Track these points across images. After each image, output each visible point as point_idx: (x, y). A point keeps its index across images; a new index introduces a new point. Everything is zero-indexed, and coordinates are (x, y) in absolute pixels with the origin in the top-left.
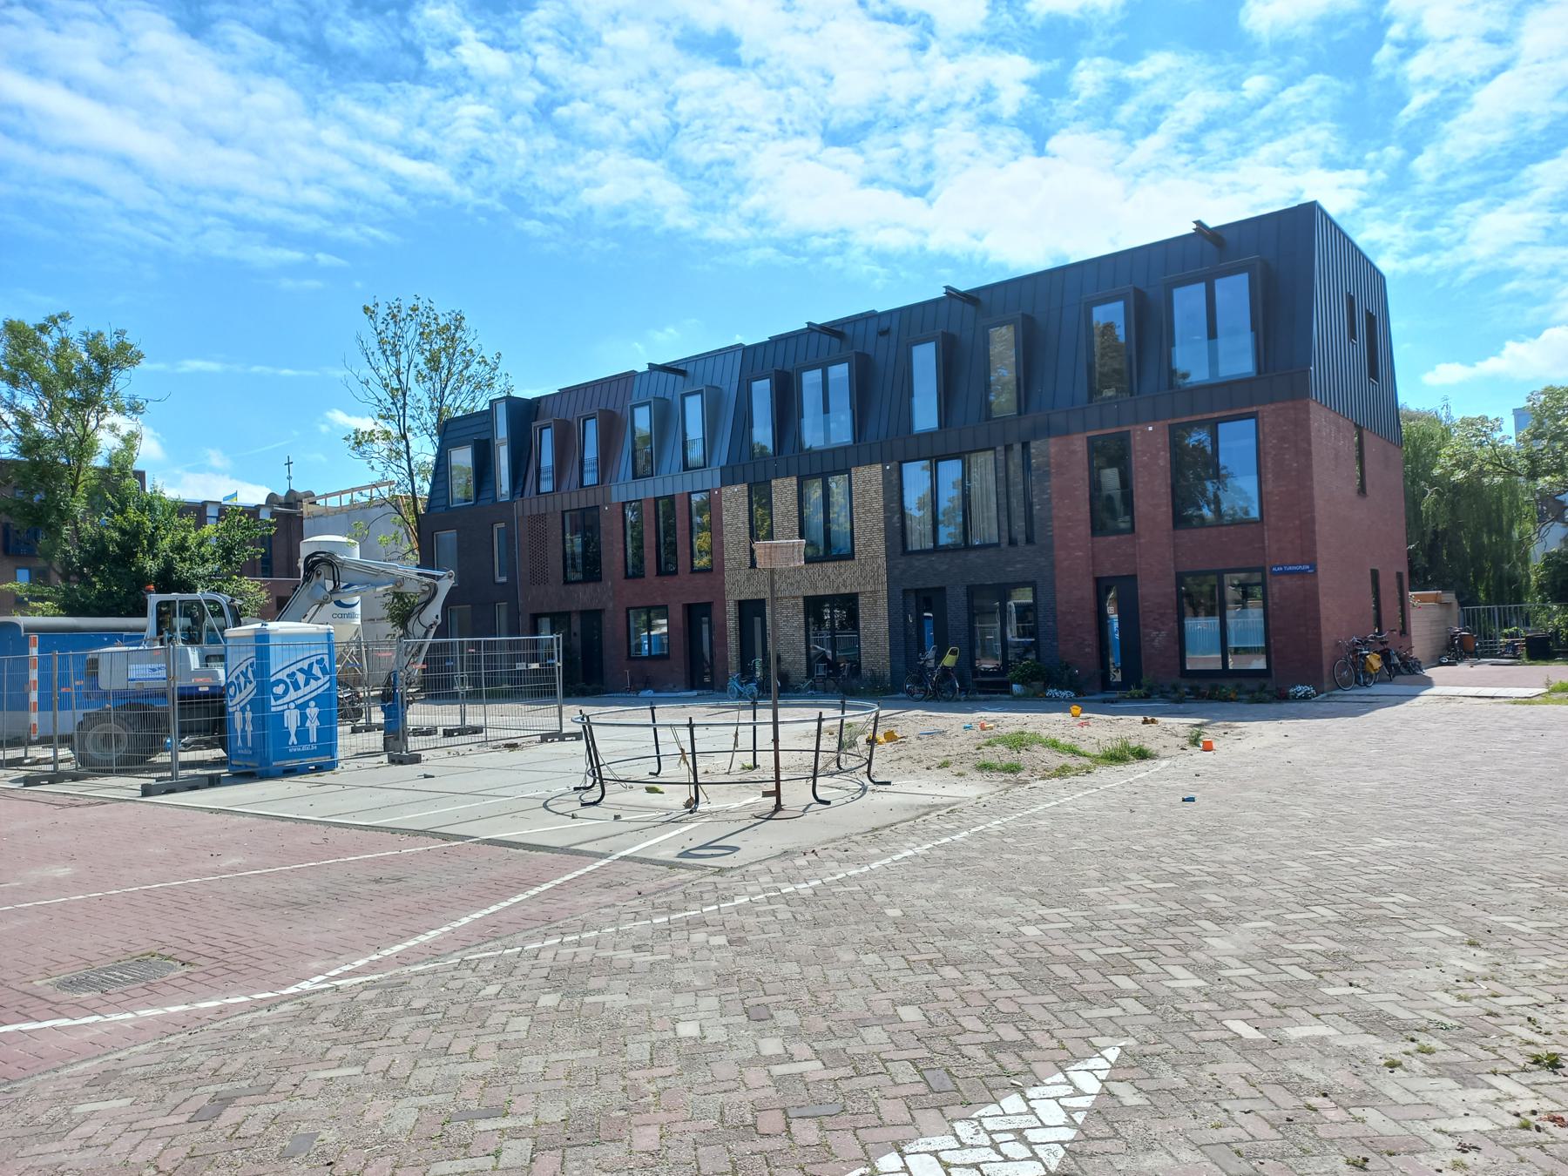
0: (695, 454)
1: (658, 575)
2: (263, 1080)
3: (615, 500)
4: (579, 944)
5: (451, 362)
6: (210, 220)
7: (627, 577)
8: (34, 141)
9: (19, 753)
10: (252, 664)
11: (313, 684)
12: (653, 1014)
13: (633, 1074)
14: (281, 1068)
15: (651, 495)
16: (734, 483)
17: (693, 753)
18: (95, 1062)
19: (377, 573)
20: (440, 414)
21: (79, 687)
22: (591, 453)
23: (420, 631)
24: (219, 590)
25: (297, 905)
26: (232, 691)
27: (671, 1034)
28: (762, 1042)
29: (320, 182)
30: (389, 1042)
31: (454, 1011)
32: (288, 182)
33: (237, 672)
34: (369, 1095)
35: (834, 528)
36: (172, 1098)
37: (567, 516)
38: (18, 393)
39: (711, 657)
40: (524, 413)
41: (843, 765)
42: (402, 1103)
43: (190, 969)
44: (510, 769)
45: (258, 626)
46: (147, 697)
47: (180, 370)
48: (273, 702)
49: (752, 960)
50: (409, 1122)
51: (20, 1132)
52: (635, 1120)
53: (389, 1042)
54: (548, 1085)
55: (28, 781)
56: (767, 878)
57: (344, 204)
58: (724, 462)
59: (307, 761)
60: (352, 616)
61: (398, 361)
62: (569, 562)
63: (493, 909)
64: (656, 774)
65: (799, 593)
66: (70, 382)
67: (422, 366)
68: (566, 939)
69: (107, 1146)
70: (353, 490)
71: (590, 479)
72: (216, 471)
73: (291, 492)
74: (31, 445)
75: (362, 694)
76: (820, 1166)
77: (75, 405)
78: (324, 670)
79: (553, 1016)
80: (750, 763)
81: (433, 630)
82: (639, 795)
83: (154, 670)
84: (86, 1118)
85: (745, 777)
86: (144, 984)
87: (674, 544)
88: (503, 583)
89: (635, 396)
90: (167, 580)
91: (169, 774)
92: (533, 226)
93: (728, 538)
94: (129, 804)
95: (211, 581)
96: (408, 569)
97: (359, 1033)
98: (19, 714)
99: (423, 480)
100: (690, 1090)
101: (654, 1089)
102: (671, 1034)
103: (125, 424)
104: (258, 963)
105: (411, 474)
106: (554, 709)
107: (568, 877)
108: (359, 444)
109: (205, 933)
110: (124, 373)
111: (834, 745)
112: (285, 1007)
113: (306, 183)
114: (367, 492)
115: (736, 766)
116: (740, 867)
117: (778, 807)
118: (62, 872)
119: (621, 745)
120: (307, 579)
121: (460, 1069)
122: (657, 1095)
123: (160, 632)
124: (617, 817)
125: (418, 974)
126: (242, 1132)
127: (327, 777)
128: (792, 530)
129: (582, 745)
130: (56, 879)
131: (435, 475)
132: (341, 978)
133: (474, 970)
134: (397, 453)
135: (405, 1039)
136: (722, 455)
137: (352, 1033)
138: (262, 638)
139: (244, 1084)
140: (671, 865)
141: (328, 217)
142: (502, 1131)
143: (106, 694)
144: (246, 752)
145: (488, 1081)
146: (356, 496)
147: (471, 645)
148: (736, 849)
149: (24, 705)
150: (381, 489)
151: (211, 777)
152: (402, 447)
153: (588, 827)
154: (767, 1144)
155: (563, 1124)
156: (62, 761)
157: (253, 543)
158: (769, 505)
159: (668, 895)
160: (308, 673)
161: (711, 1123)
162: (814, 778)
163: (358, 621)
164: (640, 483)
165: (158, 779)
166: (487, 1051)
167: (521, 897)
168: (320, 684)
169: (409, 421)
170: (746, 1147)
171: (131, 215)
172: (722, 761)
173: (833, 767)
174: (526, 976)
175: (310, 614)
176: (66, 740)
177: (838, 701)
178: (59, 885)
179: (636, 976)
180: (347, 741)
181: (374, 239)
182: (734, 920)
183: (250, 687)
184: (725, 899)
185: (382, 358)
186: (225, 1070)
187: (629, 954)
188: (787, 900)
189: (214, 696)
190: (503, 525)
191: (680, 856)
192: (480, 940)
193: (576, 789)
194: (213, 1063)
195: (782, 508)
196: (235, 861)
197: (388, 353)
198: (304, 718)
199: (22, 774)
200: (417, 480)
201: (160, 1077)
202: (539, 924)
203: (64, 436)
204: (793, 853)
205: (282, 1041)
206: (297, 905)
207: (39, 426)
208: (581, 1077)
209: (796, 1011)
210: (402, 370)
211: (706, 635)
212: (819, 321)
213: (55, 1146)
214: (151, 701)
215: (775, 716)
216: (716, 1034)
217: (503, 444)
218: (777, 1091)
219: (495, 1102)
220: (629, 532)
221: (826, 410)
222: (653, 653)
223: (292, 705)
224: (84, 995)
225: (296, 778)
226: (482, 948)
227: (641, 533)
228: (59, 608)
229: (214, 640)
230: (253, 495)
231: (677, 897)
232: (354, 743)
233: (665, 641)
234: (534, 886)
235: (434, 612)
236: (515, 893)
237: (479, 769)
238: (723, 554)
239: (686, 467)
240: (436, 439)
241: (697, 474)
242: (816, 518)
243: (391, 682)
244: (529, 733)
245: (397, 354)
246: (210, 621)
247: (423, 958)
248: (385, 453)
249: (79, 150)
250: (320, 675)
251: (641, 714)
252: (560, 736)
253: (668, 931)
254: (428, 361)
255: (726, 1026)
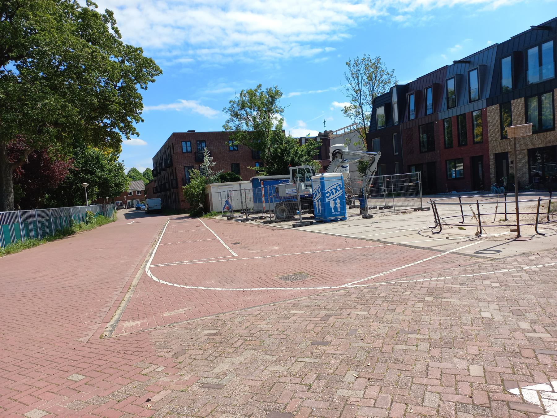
0: (475, 95)
1: (459, 146)
2: (339, 311)
3: (440, 118)
4: (438, 281)
5: (376, 77)
6: (293, 45)
7: (445, 148)
8: (246, 33)
9: (261, 215)
10: (320, 187)
11: (338, 193)
12: (470, 308)
13: (465, 327)
14: (344, 309)
15: (455, 114)
16: (493, 104)
17: (479, 214)
18: (293, 300)
19: (355, 155)
20: (373, 96)
21: (274, 196)
22: (430, 101)
23: (370, 173)
24: (308, 165)
25: (340, 261)
26: (314, 196)
27: (479, 316)
28: (520, 324)
29: (324, 22)
30: (375, 306)
31: (395, 298)
32: (315, 25)
33: (316, 190)
34: (371, 321)
35: (543, 117)
36: (315, 313)
37: (421, 127)
38: (252, 111)
39: (483, 177)
40: (403, 90)
41: (550, 219)
42: (382, 325)
43: (313, 278)
44: (404, 220)
45: (321, 175)
46: (292, 198)
47: (289, 96)
48: (326, 199)
49: (512, 293)
50: (386, 330)
51: (279, 316)
52: (467, 343)
53: (375, 306)
54: (433, 327)
55: (265, 223)
56: (516, 263)
57: (333, 28)
58: (488, 96)
59: (338, 217)
60: (346, 170)
61: (358, 79)
62: (422, 145)
63: (404, 267)
64: (462, 223)
65: (525, 148)
66: (264, 105)
67: (366, 80)
68: (432, 279)
69: (300, 323)
70: (345, 128)
71: (429, 112)
72: (302, 128)
73: (325, 131)
74: (256, 126)
75: (352, 196)
76: (553, 373)
77: (266, 112)
78: (341, 188)
79: (431, 304)
80: (504, 218)
81: (374, 173)
82: (456, 230)
83: (292, 190)
84: (294, 315)
85: (501, 224)
86: (301, 280)
87: (466, 133)
88: (397, 155)
89: (448, 76)
90: (294, 163)
91: (299, 221)
92: (399, 18)
93: (490, 128)
94: (290, 230)
95: (305, 162)
96: (364, 153)
97: (365, 301)
98: (260, 204)
99: (367, 121)
100: (489, 336)
101: (474, 333)
102: (479, 316)
103: (278, 116)
104: (331, 278)
105: (363, 119)
106: (419, 199)
107: (430, 258)
108: (346, 111)
109: (316, 268)
110: (278, 100)
111: (546, 211)
112: (341, 291)
113: (320, 23)
114: (349, 128)
115: (497, 220)
116: (502, 258)
117: (519, 236)
118: (276, 248)
119: (446, 212)
120: (333, 159)
121: (400, 317)
122: (476, 335)
123: (293, 179)
124: (447, 238)
125: (381, 285)
126: (335, 325)
127: (344, 222)
128: (522, 121)
129: (431, 212)
130: (275, 250)
131: (372, 119)
132: (357, 285)
133: (400, 286)
134: (359, 113)
135: (380, 305)
136: (487, 94)
137: (362, 301)
138: (322, 179)
139: (334, 312)
140: (472, 256)
141: (328, 34)
142: (418, 339)
143: (281, 198)
144: (320, 214)
145: (410, 322)
146: (346, 129)
147: (387, 177)
148: (500, 251)
149: (261, 202)
150: (354, 126)
151: (310, 222)
152: (360, 110)
153: (436, 241)
154: (527, 361)
155: (440, 340)
156: (272, 217)
157: (315, 149)
158: (510, 111)
159: (471, 267)
160: (336, 189)
161: (501, 349)
162: (536, 224)
163: (349, 172)
164: (451, 110)
165: (296, 223)
166: (408, 312)
167: (413, 264)
168: (340, 193)
169: (362, 101)
170: (518, 360)
171: (271, 49)
172: (491, 218)
173: (545, 220)
174: (419, 290)
175: (335, 170)
176: (272, 211)
177: (548, 192)
178: (276, 251)
179: (462, 294)
180: (349, 211)
181: (343, 38)
182: (502, 278)
183: (320, 194)
184: (497, 270)
185: (353, 80)
186: (327, 307)
187: (458, 286)
188: (527, 272)
189: (310, 197)
190: (396, 134)
191: (475, 253)
192: (401, 277)
193: (430, 227)
194: (324, 305)
195: (517, 112)
196: (320, 247)
197: (355, 78)
198: (336, 204)
199: (263, 221)
200: (366, 121)
201: (311, 307)
202: (421, 273)
203: (264, 122)
204: (529, 254)
205: (342, 301)
206: (340, 261)
207: (258, 120)
208: (445, 326)
209: (535, 314)
210: (359, 82)
211: (480, 169)
212: (537, 24)
213: (287, 321)
214: (293, 199)
215: (517, 199)
216: (498, 318)
217: (395, 103)
218: (530, 342)
219: (414, 329)
220: (446, 131)
221: (541, 64)
222: (457, 177)
223: (332, 200)
224: (287, 282)
225: (335, 223)
226: (402, 279)
227: (451, 131)
228: (267, 173)
229: (308, 180)
230: (314, 134)
231: (475, 268)
232: (351, 212)
233: (462, 172)
234: (417, 260)
235: (374, 167)
236: (411, 262)
237: (393, 220)
238: (487, 135)
239: (470, 101)
240: (371, 105)
241: (475, 104)
242: (534, 114)
243: (361, 191)
244: (410, 208)
245: (357, 77)
246: (307, 175)
247: (381, 280)
248: (355, 114)
249: (257, 32)
250: (340, 190)
251: (456, 200)
252: (422, 209)
253: (473, 280)
254: (368, 78)
255: (503, 316)
